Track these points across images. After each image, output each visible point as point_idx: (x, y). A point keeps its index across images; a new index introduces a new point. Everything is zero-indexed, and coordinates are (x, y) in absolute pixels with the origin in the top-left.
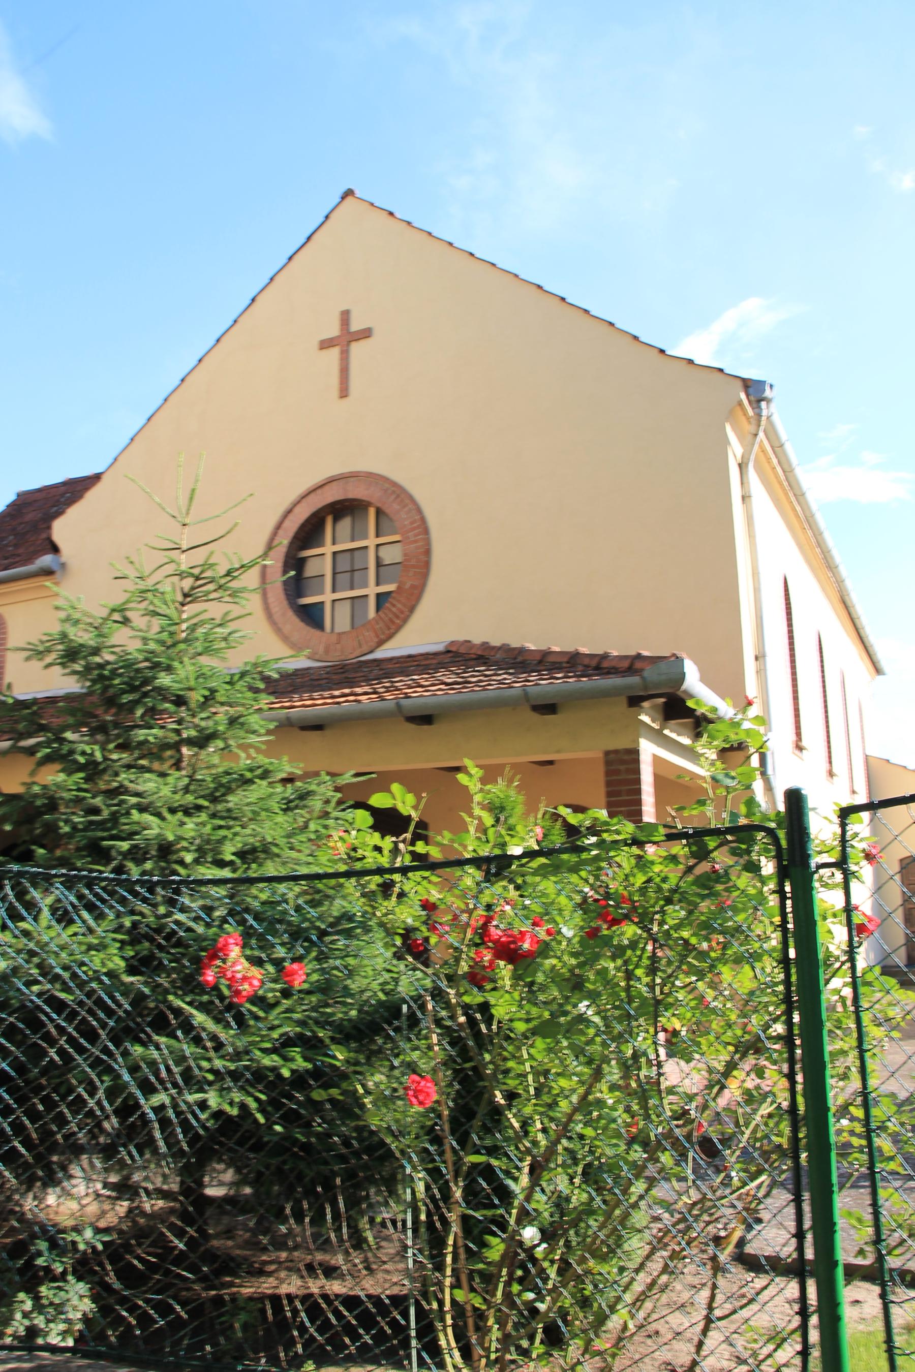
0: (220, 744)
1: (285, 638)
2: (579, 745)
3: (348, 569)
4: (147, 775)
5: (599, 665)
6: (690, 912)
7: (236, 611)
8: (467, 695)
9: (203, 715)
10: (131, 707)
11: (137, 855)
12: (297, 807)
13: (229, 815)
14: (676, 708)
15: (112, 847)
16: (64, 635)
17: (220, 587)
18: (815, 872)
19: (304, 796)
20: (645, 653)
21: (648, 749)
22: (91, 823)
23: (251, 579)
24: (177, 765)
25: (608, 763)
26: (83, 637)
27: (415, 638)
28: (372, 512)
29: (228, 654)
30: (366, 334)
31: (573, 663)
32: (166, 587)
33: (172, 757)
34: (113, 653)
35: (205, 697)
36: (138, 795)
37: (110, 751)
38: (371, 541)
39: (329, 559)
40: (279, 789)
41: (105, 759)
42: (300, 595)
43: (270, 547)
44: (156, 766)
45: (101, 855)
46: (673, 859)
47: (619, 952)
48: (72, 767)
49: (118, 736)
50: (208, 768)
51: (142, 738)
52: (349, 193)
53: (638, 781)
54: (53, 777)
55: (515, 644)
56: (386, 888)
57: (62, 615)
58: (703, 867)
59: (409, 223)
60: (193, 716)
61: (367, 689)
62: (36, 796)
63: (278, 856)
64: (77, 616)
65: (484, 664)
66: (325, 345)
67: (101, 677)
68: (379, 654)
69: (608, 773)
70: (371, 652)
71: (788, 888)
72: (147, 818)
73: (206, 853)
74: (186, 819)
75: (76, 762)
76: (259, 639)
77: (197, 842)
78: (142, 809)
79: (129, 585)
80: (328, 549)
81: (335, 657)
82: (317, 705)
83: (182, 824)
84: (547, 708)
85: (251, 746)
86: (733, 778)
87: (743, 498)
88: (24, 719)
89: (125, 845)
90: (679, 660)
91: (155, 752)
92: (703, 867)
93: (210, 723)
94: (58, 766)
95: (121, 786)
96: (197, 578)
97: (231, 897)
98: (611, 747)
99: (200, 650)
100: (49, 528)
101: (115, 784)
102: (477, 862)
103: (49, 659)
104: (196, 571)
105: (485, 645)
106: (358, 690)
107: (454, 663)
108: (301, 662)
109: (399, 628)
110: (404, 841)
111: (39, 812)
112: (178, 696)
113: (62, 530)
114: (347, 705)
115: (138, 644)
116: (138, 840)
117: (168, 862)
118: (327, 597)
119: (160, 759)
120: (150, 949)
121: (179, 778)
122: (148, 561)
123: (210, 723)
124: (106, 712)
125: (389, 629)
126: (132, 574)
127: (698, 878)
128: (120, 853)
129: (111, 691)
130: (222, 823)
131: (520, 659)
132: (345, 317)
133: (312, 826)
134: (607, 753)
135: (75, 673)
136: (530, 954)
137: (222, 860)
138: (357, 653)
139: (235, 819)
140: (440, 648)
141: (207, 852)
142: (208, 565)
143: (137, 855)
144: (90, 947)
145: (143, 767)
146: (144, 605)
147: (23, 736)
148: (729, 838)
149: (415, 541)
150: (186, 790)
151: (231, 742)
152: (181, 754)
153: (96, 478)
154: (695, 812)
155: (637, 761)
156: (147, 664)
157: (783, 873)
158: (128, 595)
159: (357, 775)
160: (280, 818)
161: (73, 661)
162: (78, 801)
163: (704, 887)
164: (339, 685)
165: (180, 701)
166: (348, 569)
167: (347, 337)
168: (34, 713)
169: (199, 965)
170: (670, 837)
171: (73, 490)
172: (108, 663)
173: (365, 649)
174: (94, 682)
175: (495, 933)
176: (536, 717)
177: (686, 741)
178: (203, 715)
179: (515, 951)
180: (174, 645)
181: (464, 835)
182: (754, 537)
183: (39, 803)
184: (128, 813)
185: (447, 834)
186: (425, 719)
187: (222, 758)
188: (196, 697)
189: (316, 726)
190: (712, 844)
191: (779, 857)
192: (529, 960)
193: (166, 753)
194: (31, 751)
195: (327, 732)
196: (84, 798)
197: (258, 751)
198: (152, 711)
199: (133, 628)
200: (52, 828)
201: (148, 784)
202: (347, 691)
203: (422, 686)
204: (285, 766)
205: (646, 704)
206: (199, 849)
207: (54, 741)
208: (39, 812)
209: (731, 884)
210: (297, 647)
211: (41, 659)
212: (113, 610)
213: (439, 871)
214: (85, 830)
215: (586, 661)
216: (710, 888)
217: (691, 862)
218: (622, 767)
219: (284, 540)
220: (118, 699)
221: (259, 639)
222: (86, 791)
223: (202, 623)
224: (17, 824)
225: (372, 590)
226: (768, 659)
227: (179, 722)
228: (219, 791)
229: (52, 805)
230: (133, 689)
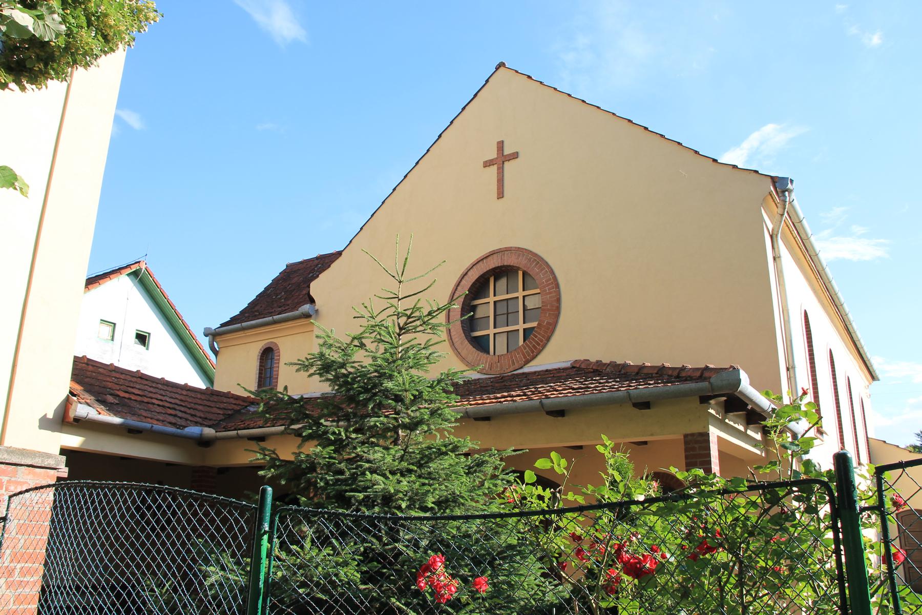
0: (426, 428)
1: (463, 359)
2: (666, 430)
3: (504, 313)
4: (376, 448)
5: (679, 375)
6: (767, 542)
7: (435, 339)
8: (588, 396)
9: (414, 408)
10: (365, 403)
11: (369, 502)
12: (475, 471)
13: (430, 476)
14: (735, 404)
15: (354, 496)
16: (322, 355)
17: (424, 323)
18: (860, 513)
19: (480, 464)
20: (711, 366)
21: (714, 433)
22: (338, 480)
23: (441, 318)
24: (395, 442)
25: (686, 443)
26: (334, 356)
27: (552, 357)
28: (520, 273)
29: (430, 367)
30: (515, 156)
31: (660, 373)
32: (389, 323)
33: (391, 437)
34: (352, 367)
35: (414, 396)
36: (368, 461)
37: (350, 432)
38: (520, 294)
39: (492, 306)
40: (463, 459)
41: (347, 437)
42: (473, 330)
43: (452, 299)
44: (381, 442)
45: (346, 502)
46: (754, 504)
47: (715, 571)
48: (326, 443)
49: (356, 423)
50: (415, 444)
51: (372, 424)
52: (501, 65)
53: (709, 455)
54: (313, 449)
55: (619, 361)
56: (547, 524)
57: (321, 341)
58: (776, 510)
59: (541, 83)
60: (407, 409)
61: (519, 393)
62: (302, 461)
63: (463, 504)
64: (330, 342)
65: (599, 375)
66: (488, 164)
67: (346, 383)
68: (526, 369)
69: (686, 450)
70: (521, 368)
71: (839, 525)
72: (376, 477)
73: (415, 502)
74: (401, 479)
75: (329, 439)
76: (445, 358)
77: (409, 494)
78: (373, 471)
79: (364, 322)
80: (491, 299)
81: (496, 372)
82: (487, 403)
83: (399, 482)
84: (644, 405)
85: (444, 429)
86: (798, 445)
87: (774, 259)
88: (295, 410)
89: (361, 496)
90: (735, 371)
91: (382, 433)
92: (776, 510)
93: (418, 414)
94: (315, 442)
95: (358, 455)
96: (409, 317)
97: (432, 532)
98: (689, 432)
99: (411, 364)
100: (309, 287)
101: (353, 455)
102: (611, 506)
103: (312, 371)
104: (408, 313)
105: (599, 362)
106: (514, 393)
107: (578, 375)
108: (473, 375)
109: (540, 352)
110: (560, 492)
111: (304, 472)
112: (396, 396)
113: (316, 288)
114: (506, 404)
115: (370, 361)
116: (370, 492)
117: (390, 508)
118: (491, 331)
119: (385, 438)
120: (377, 566)
121: (397, 451)
122: (377, 306)
123: (418, 414)
124: (349, 405)
125: (533, 352)
126: (367, 315)
127: (772, 517)
128: (357, 501)
129: (352, 393)
130: (427, 481)
131: (623, 372)
132: (501, 145)
133: (486, 485)
134: (686, 436)
135: (328, 380)
136: (650, 571)
137: (426, 507)
138: (511, 369)
139: (434, 479)
140: (568, 365)
141: (415, 500)
142: (415, 309)
143: (369, 502)
144: (338, 564)
145: (373, 443)
146: (373, 335)
147: (293, 422)
148: (795, 489)
149: (550, 293)
150: (402, 459)
151: (432, 427)
152: (398, 435)
153: (339, 254)
154: (768, 471)
155: (708, 441)
156: (376, 374)
157: (835, 515)
158: (362, 329)
159: (514, 451)
160: (464, 479)
161: (328, 372)
162: (329, 466)
163: (776, 524)
164: (500, 390)
165: (398, 399)
166: (504, 313)
167: (502, 158)
168: (301, 406)
169: (415, 578)
170: (751, 488)
171: (323, 262)
172: (350, 373)
173: (517, 366)
174: (341, 386)
175: (626, 556)
176: (636, 411)
177: (741, 428)
178: (414, 408)
179: (640, 569)
180: (394, 362)
181: (602, 488)
182: (784, 285)
183: (304, 466)
184: (363, 474)
185: (590, 487)
186: (559, 413)
187: (425, 438)
188: (409, 396)
189: (485, 418)
190: (781, 494)
191: (832, 502)
192: (650, 575)
193: (388, 434)
194: (298, 433)
195: (492, 422)
196: (334, 463)
197: (449, 433)
198: (380, 406)
199: (367, 350)
200: (312, 484)
201: (377, 454)
202: (506, 394)
203: (557, 391)
204: (469, 444)
205: (712, 402)
206: (410, 499)
207: (314, 425)
208: (304, 472)
209: (797, 522)
210: (471, 366)
211: (307, 371)
212: (354, 338)
213: (585, 512)
214: (334, 485)
215: (670, 373)
216: (781, 525)
217: (767, 506)
218: (696, 446)
219: (464, 290)
220: (359, 397)
221: (445, 358)
222: (334, 458)
223: (413, 347)
224: (289, 481)
225: (521, 326)
226: (797, 370)
227: (397, 413)
228: (424, 459)
229: (313, 468)
230: (366, 391)
